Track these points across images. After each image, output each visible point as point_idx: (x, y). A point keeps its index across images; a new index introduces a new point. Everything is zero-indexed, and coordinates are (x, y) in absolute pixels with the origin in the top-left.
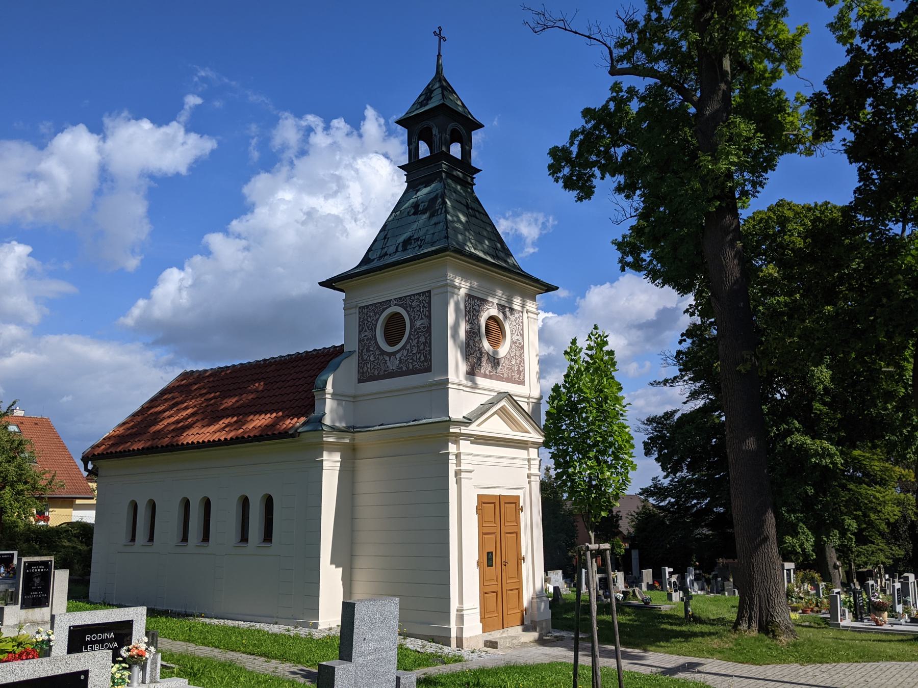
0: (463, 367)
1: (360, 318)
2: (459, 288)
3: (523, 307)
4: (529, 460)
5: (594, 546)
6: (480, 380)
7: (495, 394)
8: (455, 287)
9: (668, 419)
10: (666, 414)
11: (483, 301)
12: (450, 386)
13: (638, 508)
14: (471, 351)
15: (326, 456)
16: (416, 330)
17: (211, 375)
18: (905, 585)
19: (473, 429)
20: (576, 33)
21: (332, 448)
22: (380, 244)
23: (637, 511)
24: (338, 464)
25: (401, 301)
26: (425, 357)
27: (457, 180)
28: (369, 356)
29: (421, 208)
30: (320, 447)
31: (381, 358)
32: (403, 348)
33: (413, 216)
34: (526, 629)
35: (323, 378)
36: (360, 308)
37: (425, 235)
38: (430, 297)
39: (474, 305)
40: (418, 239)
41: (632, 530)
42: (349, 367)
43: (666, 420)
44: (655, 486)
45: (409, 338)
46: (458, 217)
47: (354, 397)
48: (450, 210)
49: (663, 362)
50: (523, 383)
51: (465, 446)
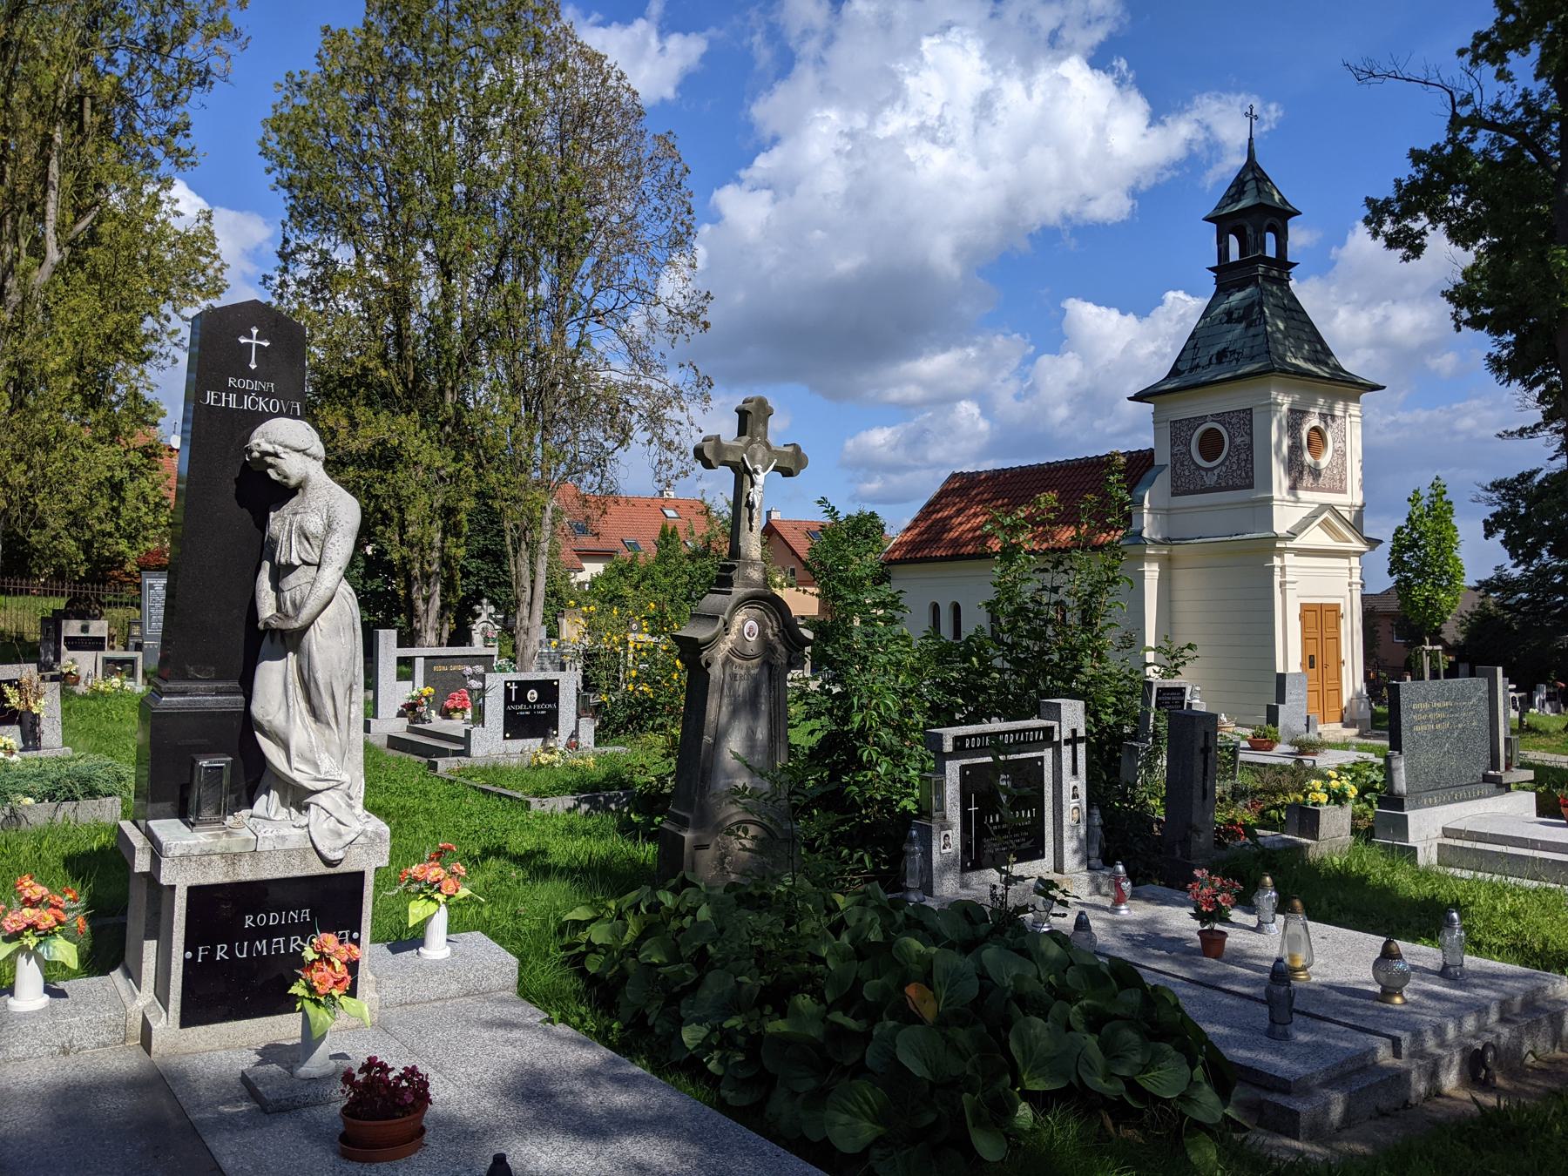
0: (1286, 483)
2: (1282, 405)
3: (1345, 412)
4: (1350, 569)
5: (1428, 647)
6: (1302, 494)
8: (1278, 404)
9: (1525, 482)
10: (1522, 475)
11: (1305, 413)
13: (1473, 606)
14: (1294, 466)
15: (1146, 567)
17: (986, 479)
19: (1298, 542)
20: (1409, 80)
21: (1152, 559)
22: (1189, 354)
23: (1471, 610)
25: (1217, 417)
26: (1247, 473)
27: (1274, 281)
29: (1235, 316)
30: (1142, 558)
32: (1222, 464)
34: (1346, 726)
35: (1140, 493)
37: (1243, 347)
38: (1251, 414)
39: (1297, 416)
40: (1234, 352)
41: (1461, 637)
42: (1163, 481)
44: (1499, 578)
45: (1228, 454)
46: (1277, 325)
48: (1269, 320)
49: (1518, 403)
50: (1344, 492)
51: (1289, 559)
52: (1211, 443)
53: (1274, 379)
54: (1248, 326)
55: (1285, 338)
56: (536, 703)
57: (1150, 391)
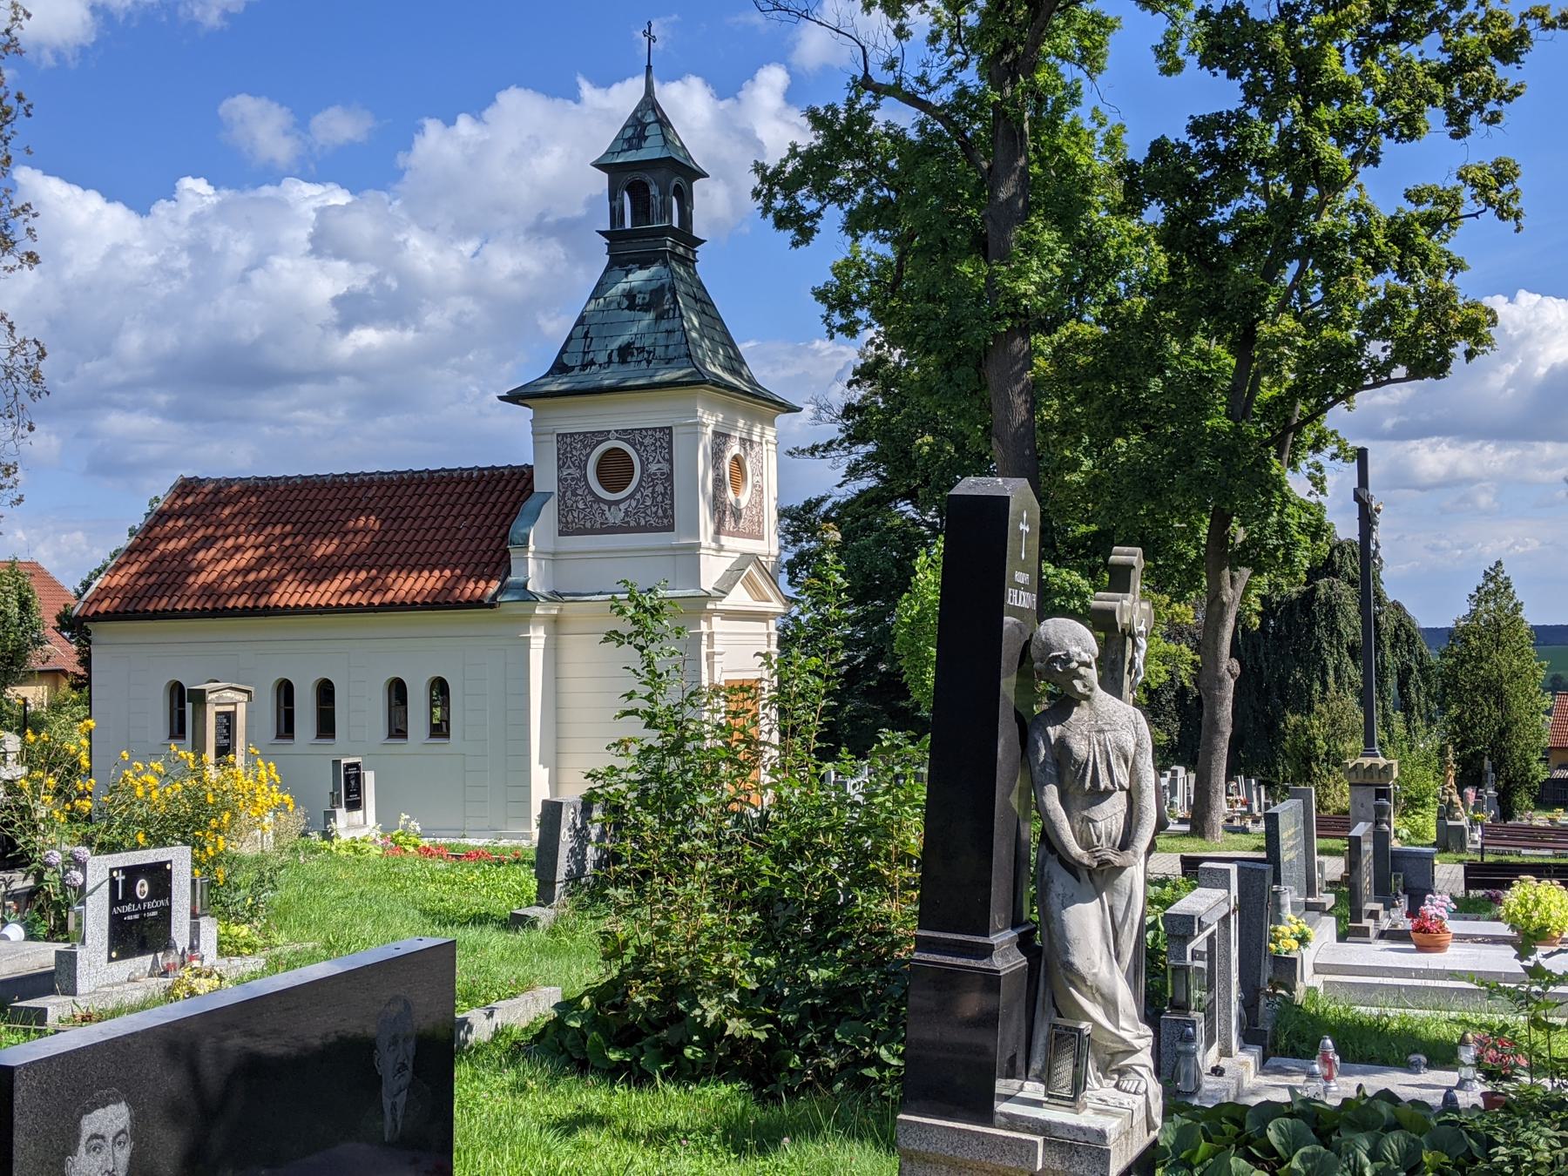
0: (711, 528)
1: (559, 449)
3: (762, 437)
4: (769, 635)
7: (738, 555)
9: (811, 511)
10: (808, 503)
12: (702, 551)
14: (719, 508)
16: (649, 475)
18: (1173, 782)
19: (729, 603)
22: (578, 345)
24: (543, 641)
25: (625, 434)
26: (665, 511)
28: (577, 502)
30: (525, 620)
31: (595, 506)
32: (631, 496)
33: (627, 311)
36: (558, 435)
37: (654, 345)
38: (671, 434)
39: (721, 437)
40: (641, 350)
43: (807, 513)
47: (554, 554)
50: (761, 538)
52: (615, 470)
53: (702, 392)
54: (659, 318)
55: (702, 337)
56: (146, 900)
57: (531, 390)
